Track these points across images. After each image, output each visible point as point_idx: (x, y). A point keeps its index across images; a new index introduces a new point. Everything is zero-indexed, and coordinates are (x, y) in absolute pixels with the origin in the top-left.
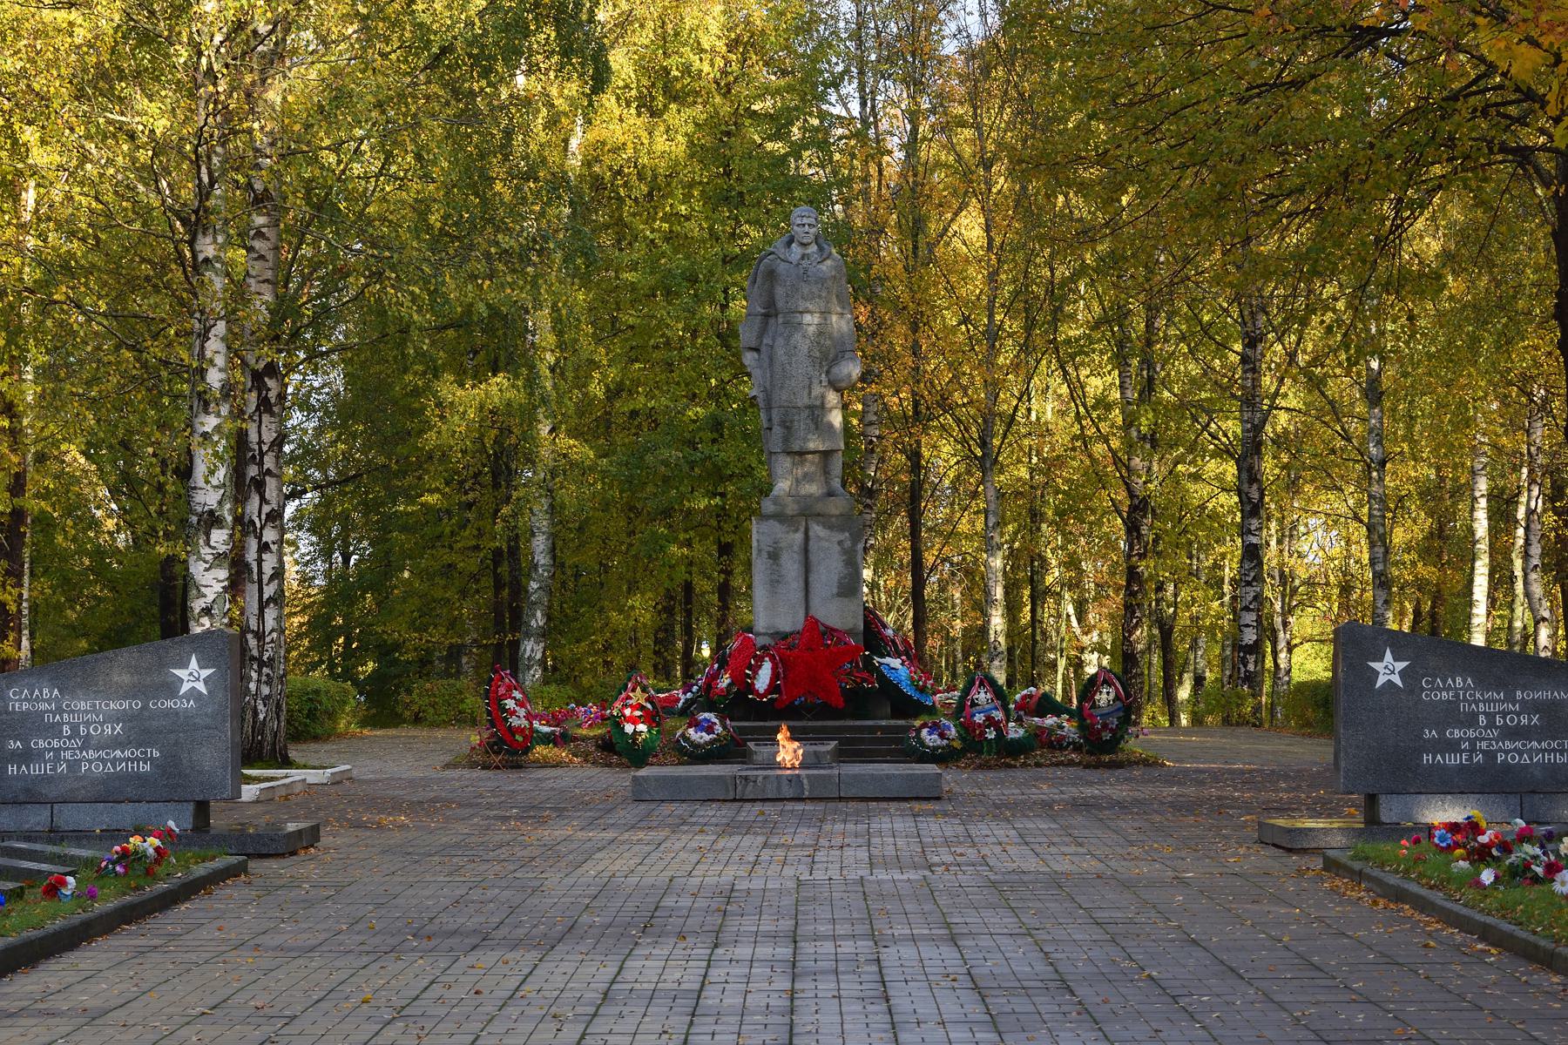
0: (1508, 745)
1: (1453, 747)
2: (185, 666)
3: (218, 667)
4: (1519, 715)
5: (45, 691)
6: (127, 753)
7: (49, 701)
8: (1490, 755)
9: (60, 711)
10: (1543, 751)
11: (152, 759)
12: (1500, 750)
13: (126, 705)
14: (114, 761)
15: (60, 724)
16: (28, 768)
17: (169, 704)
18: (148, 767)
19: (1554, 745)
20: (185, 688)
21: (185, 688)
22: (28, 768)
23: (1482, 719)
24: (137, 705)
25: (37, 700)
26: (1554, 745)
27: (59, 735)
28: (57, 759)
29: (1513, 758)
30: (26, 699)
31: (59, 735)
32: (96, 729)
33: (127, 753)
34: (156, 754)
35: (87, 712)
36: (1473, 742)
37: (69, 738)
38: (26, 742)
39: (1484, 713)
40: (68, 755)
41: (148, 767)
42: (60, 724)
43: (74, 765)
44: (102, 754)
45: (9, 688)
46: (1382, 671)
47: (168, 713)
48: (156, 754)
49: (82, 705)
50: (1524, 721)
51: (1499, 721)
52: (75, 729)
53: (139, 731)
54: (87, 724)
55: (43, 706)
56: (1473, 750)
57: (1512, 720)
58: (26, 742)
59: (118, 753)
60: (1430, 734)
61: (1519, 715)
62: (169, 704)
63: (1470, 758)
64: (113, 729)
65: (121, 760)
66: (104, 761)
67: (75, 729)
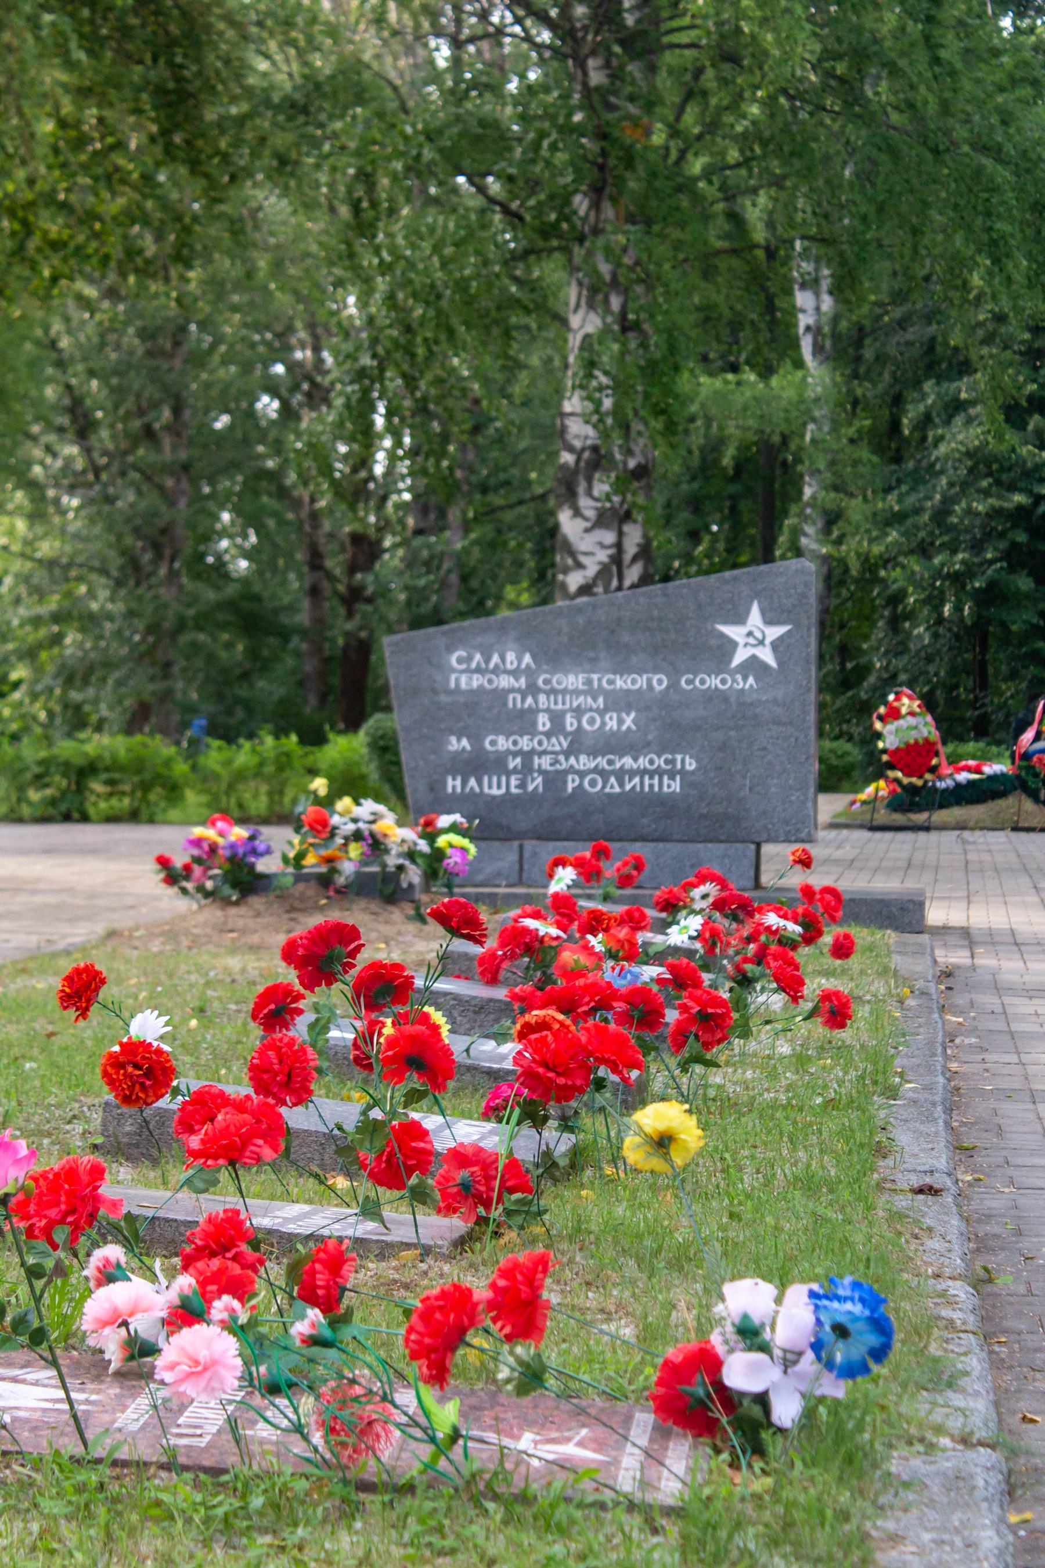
0: (584, 762)
1: (497, 765)
2: (740, 619)
3: (797, 624)
4: (602, 713)
5: (511, 656)
6: (643, 762)
7: (515, 673)
8: (554, 780)
9: (533, 689)
10: (642, 773)
11: (683, 772)
12: (571, 770)
13: (641, 682)
14: (621, 775)
15: (534, 712)
16: (480, 783)
17: (714, 682)
18: (676, 786)
19: (660, 762)
20: (740, 657)
21: (740, 657)
22: (480, 783)
23: (543, 722)
24: (660, 682)
25: (496, 671)
26: (660, 762)
27: (531, 729)
28: (527, 769)
29: (593, 783)
30: (478, 670)
31: (531, 729)
32: (592, 721)
33: (643, 762)
34: (691, 765)
35: (577, 692)
36: (528, 756)
37: (548, 735)
38: (476, 739)
39: (547, 710)
40: (545, 762)
41: (676, 786)
42: (534, 712)
43: (554, 780)
44: (602, 762)
45: (450, 649)
46: (741, 640)
47: (712, 696)
48: (691, 765)
49: (573, 680)
50: (612, 724)
51: (570, 723)
52: (557, 719)
53: (669, 725)
54: (578, 712)
55: (505, 682)
56: (527, 769)
57: (592, 721)
58: (476, 739)
59: (628, 762)
60: (457, 744)
61: (602, 713)
62: (714, 682)
63: (522, 785)
64: (621, 722)
65: (632, 773)
66: (604, 774)
67: (557, 719)
